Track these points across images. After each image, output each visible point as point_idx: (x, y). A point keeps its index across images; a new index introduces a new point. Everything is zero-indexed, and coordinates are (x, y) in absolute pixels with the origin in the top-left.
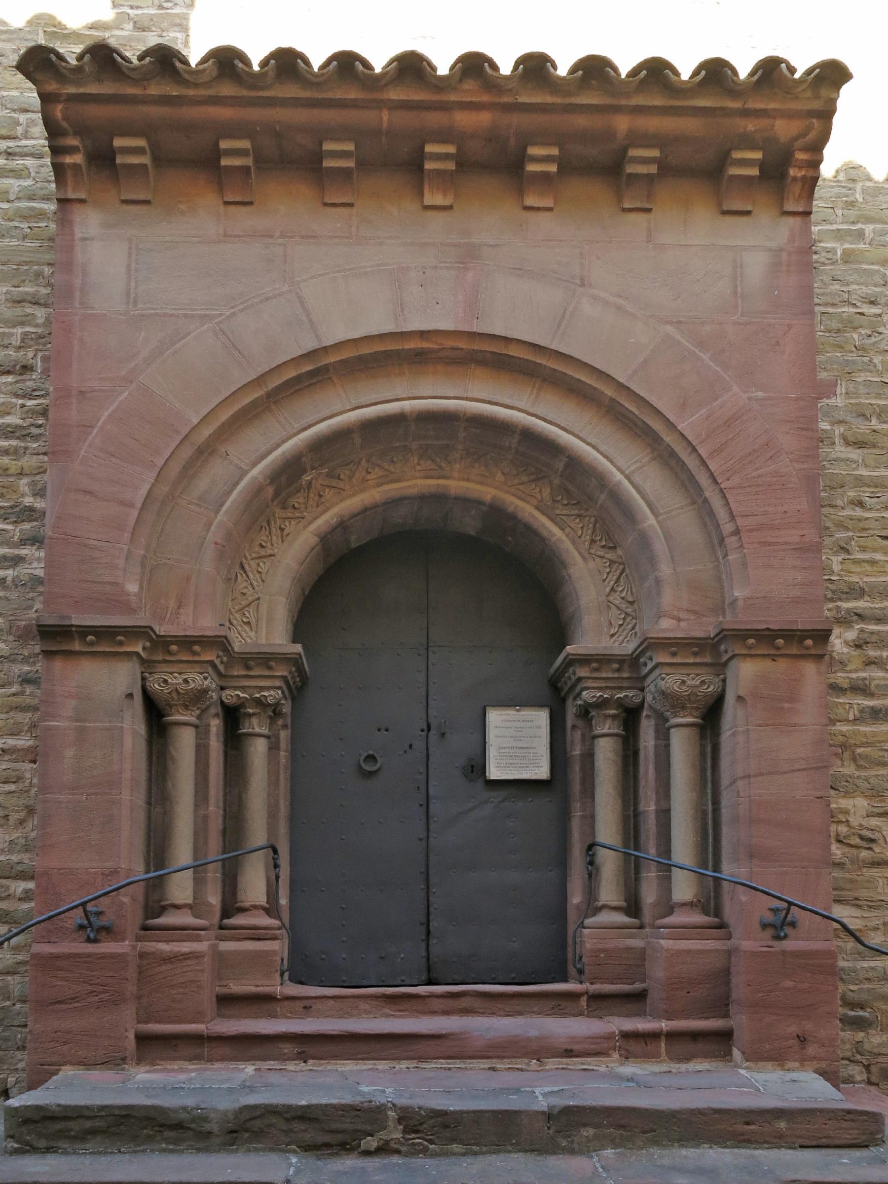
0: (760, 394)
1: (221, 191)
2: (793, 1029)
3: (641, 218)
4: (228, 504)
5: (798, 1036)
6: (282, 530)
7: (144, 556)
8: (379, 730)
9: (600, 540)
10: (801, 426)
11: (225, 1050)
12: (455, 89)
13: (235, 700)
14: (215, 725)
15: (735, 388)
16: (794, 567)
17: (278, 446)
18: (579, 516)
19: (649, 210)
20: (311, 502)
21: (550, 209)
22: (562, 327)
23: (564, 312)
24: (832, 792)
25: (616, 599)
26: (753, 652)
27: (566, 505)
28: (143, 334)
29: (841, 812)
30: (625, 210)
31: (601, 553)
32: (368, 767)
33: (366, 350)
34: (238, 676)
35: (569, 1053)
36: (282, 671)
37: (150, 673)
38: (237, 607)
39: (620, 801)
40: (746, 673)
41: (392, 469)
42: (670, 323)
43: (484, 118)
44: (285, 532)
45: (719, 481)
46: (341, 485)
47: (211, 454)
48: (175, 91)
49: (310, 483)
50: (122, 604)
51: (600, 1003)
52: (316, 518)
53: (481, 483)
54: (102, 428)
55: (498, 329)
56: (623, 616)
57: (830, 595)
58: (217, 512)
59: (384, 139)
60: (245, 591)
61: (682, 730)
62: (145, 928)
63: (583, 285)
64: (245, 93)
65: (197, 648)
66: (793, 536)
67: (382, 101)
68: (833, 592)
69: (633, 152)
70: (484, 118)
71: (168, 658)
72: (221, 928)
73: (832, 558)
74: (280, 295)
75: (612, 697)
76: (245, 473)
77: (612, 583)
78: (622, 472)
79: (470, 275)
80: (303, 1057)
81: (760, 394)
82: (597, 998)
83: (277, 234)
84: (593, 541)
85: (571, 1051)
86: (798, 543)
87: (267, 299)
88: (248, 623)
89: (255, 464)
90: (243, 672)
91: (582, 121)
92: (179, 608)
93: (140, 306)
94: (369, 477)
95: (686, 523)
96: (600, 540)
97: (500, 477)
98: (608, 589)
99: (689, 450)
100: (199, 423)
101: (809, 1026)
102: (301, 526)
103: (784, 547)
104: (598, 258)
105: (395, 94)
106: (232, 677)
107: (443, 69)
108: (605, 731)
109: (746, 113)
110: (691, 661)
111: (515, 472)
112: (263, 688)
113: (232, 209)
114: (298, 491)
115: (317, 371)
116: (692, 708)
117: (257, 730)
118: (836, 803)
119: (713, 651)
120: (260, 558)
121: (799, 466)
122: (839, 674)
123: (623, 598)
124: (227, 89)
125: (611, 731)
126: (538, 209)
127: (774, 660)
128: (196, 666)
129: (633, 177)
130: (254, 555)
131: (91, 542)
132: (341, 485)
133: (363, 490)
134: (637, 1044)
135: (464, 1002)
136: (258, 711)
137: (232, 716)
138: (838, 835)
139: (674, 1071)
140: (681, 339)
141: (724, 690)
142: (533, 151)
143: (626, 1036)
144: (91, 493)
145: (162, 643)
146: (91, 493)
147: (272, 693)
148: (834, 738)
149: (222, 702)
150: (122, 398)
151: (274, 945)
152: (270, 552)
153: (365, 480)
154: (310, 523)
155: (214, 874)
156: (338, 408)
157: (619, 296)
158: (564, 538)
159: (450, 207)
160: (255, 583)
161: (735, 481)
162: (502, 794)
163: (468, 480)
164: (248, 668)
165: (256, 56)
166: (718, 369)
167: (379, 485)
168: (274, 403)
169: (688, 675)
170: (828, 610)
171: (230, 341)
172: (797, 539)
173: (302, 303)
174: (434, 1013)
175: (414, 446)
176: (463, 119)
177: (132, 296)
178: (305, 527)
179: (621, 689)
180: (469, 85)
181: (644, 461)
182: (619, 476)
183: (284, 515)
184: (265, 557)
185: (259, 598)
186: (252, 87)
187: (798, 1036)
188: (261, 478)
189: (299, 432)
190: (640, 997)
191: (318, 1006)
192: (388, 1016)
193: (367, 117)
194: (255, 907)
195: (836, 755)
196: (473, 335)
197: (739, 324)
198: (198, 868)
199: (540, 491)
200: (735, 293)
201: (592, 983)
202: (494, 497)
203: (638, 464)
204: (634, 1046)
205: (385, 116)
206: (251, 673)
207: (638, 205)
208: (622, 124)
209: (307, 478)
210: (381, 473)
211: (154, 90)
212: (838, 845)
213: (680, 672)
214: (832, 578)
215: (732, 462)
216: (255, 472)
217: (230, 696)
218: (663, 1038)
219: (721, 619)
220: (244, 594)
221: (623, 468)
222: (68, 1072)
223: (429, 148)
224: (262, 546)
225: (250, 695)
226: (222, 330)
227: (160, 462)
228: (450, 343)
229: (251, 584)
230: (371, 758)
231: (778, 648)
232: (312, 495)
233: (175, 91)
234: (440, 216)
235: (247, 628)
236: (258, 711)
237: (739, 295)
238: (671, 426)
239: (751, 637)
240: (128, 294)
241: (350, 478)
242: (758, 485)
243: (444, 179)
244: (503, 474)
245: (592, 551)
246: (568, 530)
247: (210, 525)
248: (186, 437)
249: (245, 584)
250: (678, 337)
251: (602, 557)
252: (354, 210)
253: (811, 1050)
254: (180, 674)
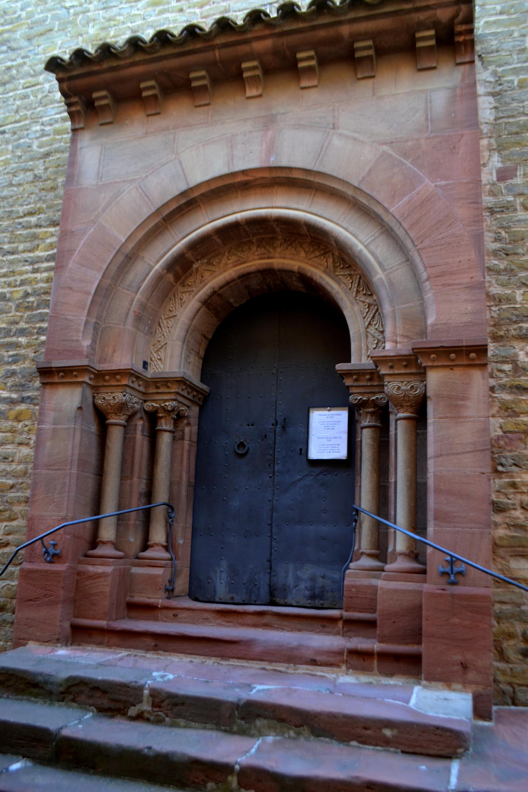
0: (444, 183)
1: (356, 72)
2: (458, 658)
3: (370, 82)
4: (142, 288)
5: (462, 664)
6: (181, 299)
7: (96, 323)
8: (248, 425)
9: (363, 290)
10: (470, 201)
11: (115, 640)
12: (251, 31)
13: (151, 408)
14: (140, 424)
15: (427, 180)
16: (466, 300)
17: (170, 249)
18: (350, 275)
19: (373, 77)
20: (198, 281)
21: (316, 86)
22: (321, 156)
23: (322, 147)
24: (514, 468)
25: (372, 330)
26: (436, 364)
27: (343, 268)
28: (103, 195)
29: (524, 485)
30: (359, 79)
31: (363, 299)
32: (241, 452)
33: (213, 186)
34: (153, 393)
35: (314, 662)
36: (174, 388)
37: (97, 394)
38: (155, 350)
39: (376, 475)
40: (435, 379)
41: (242, 255)
42: (386, 143)
43: (268, 43)
44: (183, 301)
45: (416, 244)
46: (214, 269)
47: (136, 259)
48: (115, 64)
49: (197, 269)
50: (76, 353)
51: (352, 625)
52: (199, 291)
53: (292, 259)
54: (79, 251)
55: (284, 163)
56: (376, 342)
57: (514, 319)
58: (136, 293)
59: (219, 65)
60: (160, 339)
61: (402, 421)
62: (86, 556)
63: (334, 128)
64: (147, 57)
65: (118, 377)
66: (465, 279)
67: (213, 46)
68: (517, 316)
69: (357, 45)
70: (268, 43)
71: (105, 384)
72: (138, 558)
73: (517, 291)
74: (171, 161)
75: (369, 400)
76: (152, 268)
77: (369, 319)
78: (363, 243)
79: (270, 133)
80: (156, 648)
81: (444, 183)
82: (349, 622)
83: (171, 128)
84: (358, 292)
85: (315, 661)
86: (468, 283)
87: (163, 165)
88: (160, 359)
89: (158, 262)
90: (155, 391)
91: (322, 33)
92: (113, 353)
93: (103, 179)
94: (229, 262)
95: (401, 274)
96: (363, 290)
97: (303, 254)
98: (367, 323)
99: (398, 225)
100: (126, 241)
101: (469, 656)
102: (191, 296)
103: (459, 287)
104: (343, 111)
105: (219, 41)
106: (150, 394)
107: (240, 22)
108: (366, 424)
109: (314, 28)
110: (403, 371)
111: (312, 250)
112: (166, 401)
113: (151, 118)
114: (191, 275)
115: (189, 203)
116: (407, 406)
117: (164, 427)
118: (520, 478)
119: (415, 362)
120: (169, 318)
121: (469, 229)
122: (522, 378)
123: (376, 329)
124: (138, 57)
125: (371, 424)
126: (309, 88)
127: (452, 369)
128: (120, 388)
129: (195, 88)
130: (166, 317)
131: (69, 317)
132: (214, 269)
133: (225, 271)
134: (358, 659)
135: (266, 620)
136: (164, 415)
137: (152, 418)
138: (522, 503)
139: (375, 682)
140: (392, 153)
141: (426, 390)
142: (300, 55)
143: (354, 653)
144: (70, 288)
145: (100, 375)
146: (70, 288)
147: (171, 403)
148: (518, 426)
149: (144, 410)
150: (90, 232)
151: (159, 571)
152: (174, 314)
153: (226, 264)
154: (196, 294)
155: (135, 520)
156: (203, 222)
157: (355, 131)
158: (340, 291)
159: (260, 96)
160: (165, 334)
161: (427, 243)
162: (317, 470)
163: (284, 258)
164: (158, 388)
165: (91, 50)
166: (416, 169)
167: (235, 266)
168: (170, 224)
169: (403, 382)
170: (515, 330)
171: (143, 191)
172: (467, 280)
173: (181, 164)
174: (248, 625)
175: (255, 240)
176: (258, 46)
177: (100, 175)
178: (193, 297)
179: (374, 393)
180: (258, 27)
181: (376, 235)
182: (360, 247)
183: (182, 290)
184: (171, 317)
185: (166, 344)
186: (149, 54)
187: (462, 664)
188: (160, 270)
189: (182, 239)
190: (371, 624)
191: (183, 615)
192: (220, 625)
193: (208, 56)
194: (157, 544)
195: (520, 439)
196: (271, 169)
197: (429, 138)
198: (120, 518)
199: (327, 261)
200: (427, 119)
201: (346, 611)
202: (299, 268)
203: (373, 238)
204: (355, 661)
205: (217, 53)
206: (159, 391)
207: (367, 75)
208: (345, 30)
209: (195, 266)
210: (236, 259)
211: (105, 65)
212: (522, 511)
213: (397, 380)
214: (517, 306)
215: (425, 230)
216: (157, 267)
217: (149, 406)
218: (376, 657)
219: (424, 340)
220: (159, 341)
221: (363, 241)
222: (32, 645)
223: (244, 65)
224: (170, 311)
225: (160, 405)
226: (140, 186)
227: (105, 267)
228: (259, 175)
229: (163, 335)
230: (241, 445)
231: (453, 360)
232: (198, 277)
233: (115, 64)
234: (257, 101)
235: (159, 362)
236: (164, 415)
237: (429, 120)
238: (386, 210)
239: (433, 353)
240: (98, 174)
241: (219, 263)
242: (442, 245)
243: (255, 79)
244: (305, 252)
245: (358, 298)
246: (343, 285)
247: (133, 301)
248: (118, 251)
249: (160, 335)
250: (391, 152)
251: (364, 302)
252: (211, 107)
253: (471, 675)
254: (112, 393)
